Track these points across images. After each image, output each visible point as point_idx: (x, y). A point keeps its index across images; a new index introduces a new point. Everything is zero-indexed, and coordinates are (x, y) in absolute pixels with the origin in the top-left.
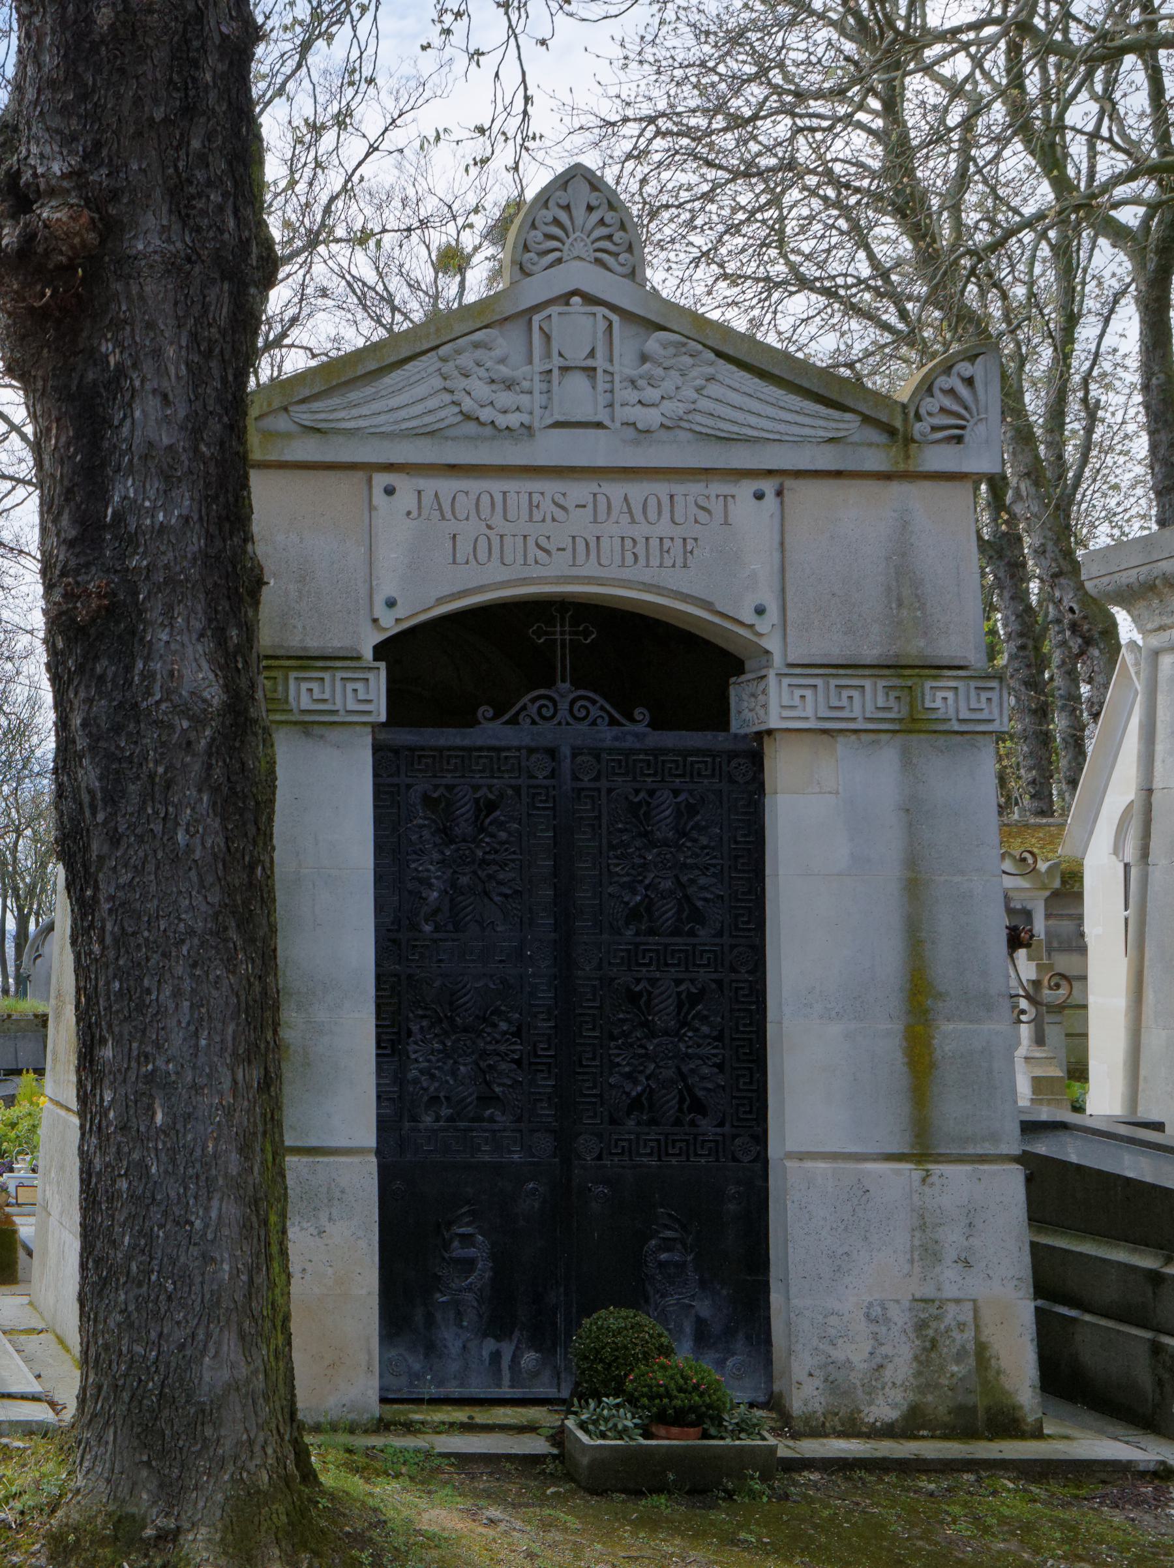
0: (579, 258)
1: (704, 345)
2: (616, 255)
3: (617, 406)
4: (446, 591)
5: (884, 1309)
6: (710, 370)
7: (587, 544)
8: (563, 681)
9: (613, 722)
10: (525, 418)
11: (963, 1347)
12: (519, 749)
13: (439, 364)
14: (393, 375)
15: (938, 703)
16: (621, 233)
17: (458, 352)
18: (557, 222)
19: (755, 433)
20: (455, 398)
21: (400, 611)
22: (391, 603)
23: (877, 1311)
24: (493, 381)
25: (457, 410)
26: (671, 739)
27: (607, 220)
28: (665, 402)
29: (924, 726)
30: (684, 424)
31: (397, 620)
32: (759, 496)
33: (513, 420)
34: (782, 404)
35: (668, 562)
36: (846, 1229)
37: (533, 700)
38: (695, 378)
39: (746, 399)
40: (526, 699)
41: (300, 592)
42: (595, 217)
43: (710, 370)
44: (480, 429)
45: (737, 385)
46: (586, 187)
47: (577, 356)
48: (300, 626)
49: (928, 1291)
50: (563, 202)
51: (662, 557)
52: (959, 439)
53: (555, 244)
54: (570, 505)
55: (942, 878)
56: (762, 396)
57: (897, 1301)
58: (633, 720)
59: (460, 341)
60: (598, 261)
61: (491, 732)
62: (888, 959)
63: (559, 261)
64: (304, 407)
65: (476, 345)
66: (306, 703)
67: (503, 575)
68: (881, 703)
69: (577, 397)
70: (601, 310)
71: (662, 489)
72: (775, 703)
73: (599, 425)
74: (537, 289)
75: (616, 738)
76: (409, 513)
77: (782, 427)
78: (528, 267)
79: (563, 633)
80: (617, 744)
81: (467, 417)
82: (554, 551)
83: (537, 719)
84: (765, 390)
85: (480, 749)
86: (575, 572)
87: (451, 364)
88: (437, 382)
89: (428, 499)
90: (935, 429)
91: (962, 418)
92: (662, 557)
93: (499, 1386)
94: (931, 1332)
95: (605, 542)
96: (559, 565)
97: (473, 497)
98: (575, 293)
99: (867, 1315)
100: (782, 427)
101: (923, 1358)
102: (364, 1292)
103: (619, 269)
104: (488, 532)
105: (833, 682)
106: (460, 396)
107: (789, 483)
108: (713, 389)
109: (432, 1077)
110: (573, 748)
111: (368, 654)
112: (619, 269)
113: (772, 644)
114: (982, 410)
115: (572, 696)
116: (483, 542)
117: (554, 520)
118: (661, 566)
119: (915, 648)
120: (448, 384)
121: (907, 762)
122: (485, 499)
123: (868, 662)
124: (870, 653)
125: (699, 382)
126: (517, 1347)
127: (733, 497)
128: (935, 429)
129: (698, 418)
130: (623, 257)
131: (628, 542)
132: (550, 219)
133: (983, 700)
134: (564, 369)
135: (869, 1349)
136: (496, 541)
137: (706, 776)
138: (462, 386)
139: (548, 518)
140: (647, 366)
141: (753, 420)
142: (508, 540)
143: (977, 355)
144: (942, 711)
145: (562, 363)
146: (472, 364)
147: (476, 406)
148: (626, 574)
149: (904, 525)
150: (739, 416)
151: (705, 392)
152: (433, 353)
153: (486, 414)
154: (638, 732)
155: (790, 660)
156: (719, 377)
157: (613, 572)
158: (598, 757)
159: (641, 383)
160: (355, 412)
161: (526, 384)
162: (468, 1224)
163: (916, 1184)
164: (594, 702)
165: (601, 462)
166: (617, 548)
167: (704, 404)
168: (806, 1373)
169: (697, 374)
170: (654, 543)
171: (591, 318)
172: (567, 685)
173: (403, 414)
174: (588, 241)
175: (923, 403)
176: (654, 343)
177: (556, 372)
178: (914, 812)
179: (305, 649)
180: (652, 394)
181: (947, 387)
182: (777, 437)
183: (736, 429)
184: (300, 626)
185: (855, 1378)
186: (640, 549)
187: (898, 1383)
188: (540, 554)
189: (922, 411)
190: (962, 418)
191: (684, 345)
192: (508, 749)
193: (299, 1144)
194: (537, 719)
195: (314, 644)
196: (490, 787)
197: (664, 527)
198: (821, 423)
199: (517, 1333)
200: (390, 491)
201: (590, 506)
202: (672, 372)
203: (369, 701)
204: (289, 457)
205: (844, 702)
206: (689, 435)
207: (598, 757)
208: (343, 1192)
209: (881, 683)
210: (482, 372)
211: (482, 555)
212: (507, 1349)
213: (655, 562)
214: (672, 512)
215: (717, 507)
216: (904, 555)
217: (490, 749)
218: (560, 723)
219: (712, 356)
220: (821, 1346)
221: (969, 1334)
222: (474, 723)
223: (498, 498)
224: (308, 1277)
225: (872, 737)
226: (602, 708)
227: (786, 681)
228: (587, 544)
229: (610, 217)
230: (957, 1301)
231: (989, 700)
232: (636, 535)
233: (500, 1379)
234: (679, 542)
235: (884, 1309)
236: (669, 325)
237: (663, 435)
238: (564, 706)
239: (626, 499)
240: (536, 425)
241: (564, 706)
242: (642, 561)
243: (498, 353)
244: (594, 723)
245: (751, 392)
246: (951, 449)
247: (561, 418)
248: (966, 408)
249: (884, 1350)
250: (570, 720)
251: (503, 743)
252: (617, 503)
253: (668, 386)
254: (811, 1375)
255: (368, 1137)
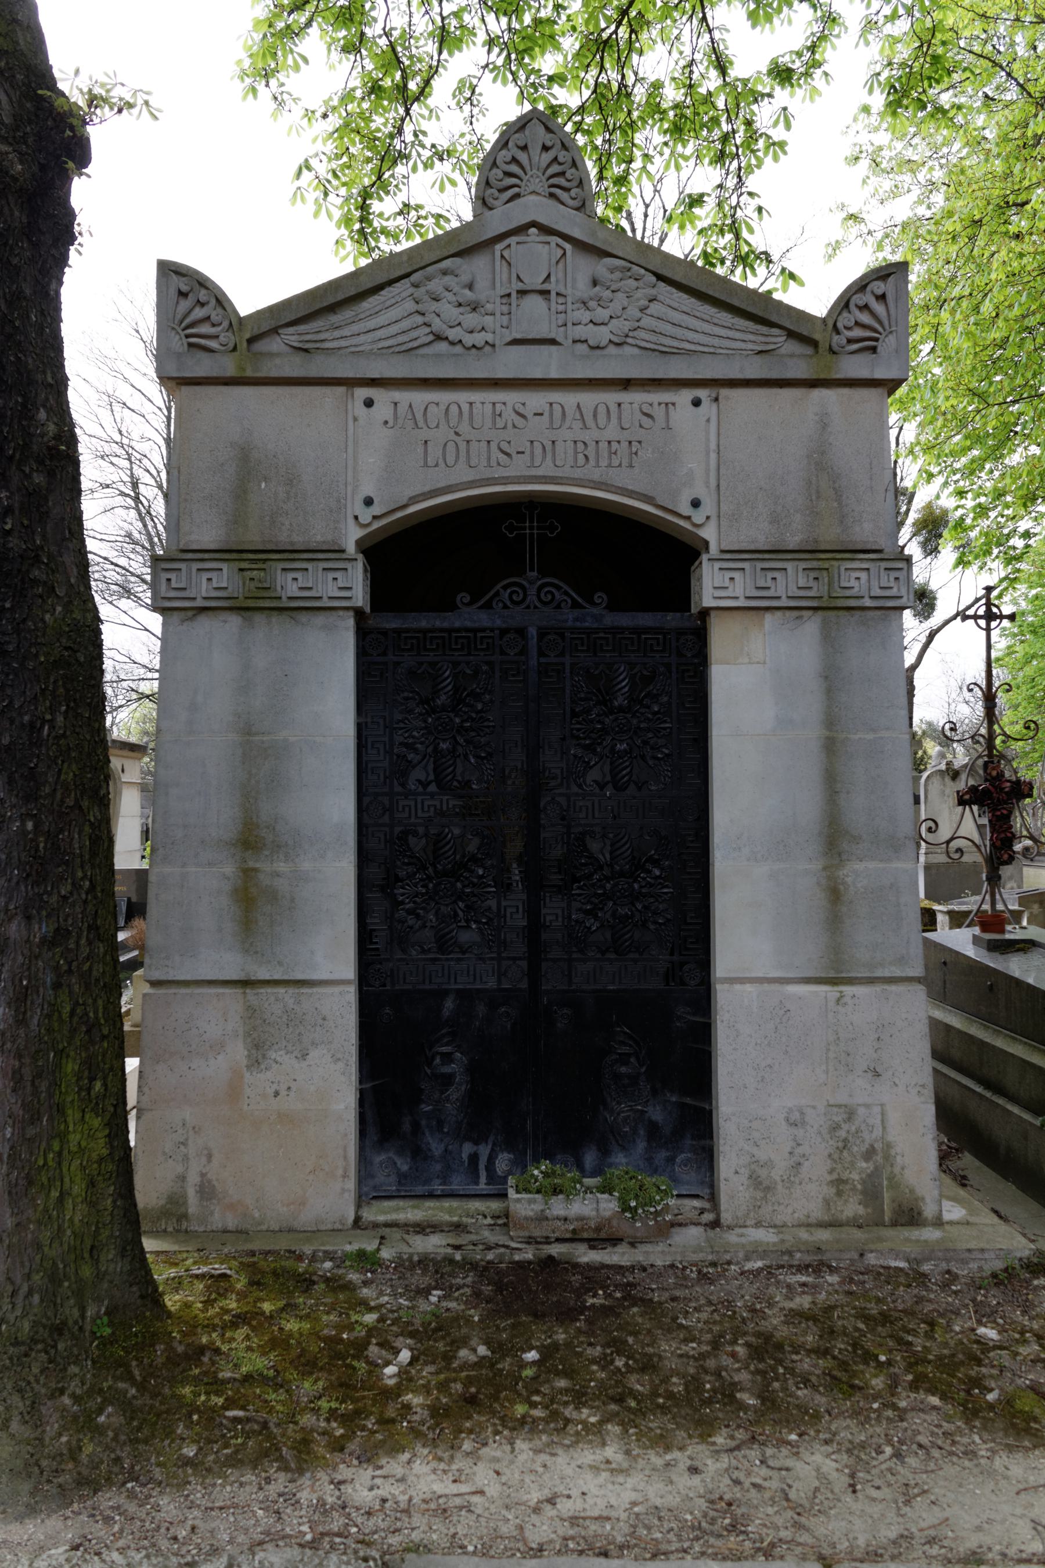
0: (533, 192)
1: (647, 270)
2: (567, 190)
3: (569, 325)
4: (418, 489)
5: (802, 1113)
6: (653, 292)
7: (544, 447)
8: (532, 570)
9: (575, 605)
10: (489, 337)
11: (872, 1146)
12: (492, 630)
13: (412, 290)
14: (371, 300)
15: (853, 583)
16: (573, 170)
17: (429, 279)
18: (514, 160)
19: (692, 347)
20: (426, 319)
21: (376, 509)
22: (369, 502)
23: (796, 1116)
24: (460, 305)
25: (428, 330)
26: (625, 620)
27: (561, 159)
28: (613, 321)
29: (840, 603)
30: (629, 340)
31: (375, 517)
32: (697, 403)
33: (479, 339)
34: (716, 321)
35: (616, 463)
36: (769, 1044)
37: (505, 588)
38: (638, 300)
39: (685, 317)
40: (498, 587)
41: (288, 493)
42: (547, 157)
43: (653, 292)
44: (451, 348)
45: (675, 305)
46: (541, 130)
47: (534, 281)
48: (287, 523)
49: (842, 1098)
50: (521, 143)
51: (610, 458)
52: (874, 350)
53: (514, 181)
54: (528, 412)
55: (857, 737)
56: (698, 314)
57: (814, 1107)
58: (593, 604)
59: (429, 269)
60: (552, 195)
61: (469, 617)
62: (808, 806)
63: (517, 196)
64: (291, 330)
65: (445, 273)
66: (293, 590)
67: (469, 476)
68: (802, 583)
69: (535, 316)
70: (554, 240)
71: (611, 397)
72: (712, 585)
73: (553, 342)
74: (500, 220)
75: (576, 619)
76: (386, 422)
77: (716, 342)
78: (490, 201)
79: (531, 528)
80: (578, 624)
81: (439, 337)
82: (514, 455)
83: (508, 603)
84: (701, 308)
85: (458, 630)
86: (533, 472)
87: (422, 290)
88: (410, 306)
89: (403, 409)
90: (850, 341)
91: (876, 331)
92: (610, 458)
93: (477, 1183)
94: (843, 1134)
95: (559, 445)
96: (518, 467)
97: (443, 407)
98: (534, 224)
99: (787, 1120)
100: (716, 342)
101: (836, 1156)
102: (342, 1106)
103: (571, 202)
104: (456, 438)
105: (760, 565)
106: (430, 318)
107: (724, 392)
108: (655, 308)
109: (418, 916)
110: (539, 628)
111: (351, 548)
112: (571, 202)
113: (708, 533)
114: (893, 323)
115: (539, 583)
116: (451, 447)
117: (514, 426)
118: (609, 466)
119: (829, 535)
120: (420, 307)
121: (828, 639)
122: (454, 409)
123: (791, 548)
124: (793, 541)
125: (644, 302)
126: (492, 1150)
127: (673, 404)
128: (850, 341)
129: (642, 334)
130: (573, 193)
131: (580, 446)
132: (509, 159)
133: (892, 579)
134: (522, 293)
135: (789, 1149)
136: (463, 446)
137: (582, 651)
138: (433, 308)
139: (510, 425)
140: (597, 288)
141: (691, 336)
142: (474, 445)
143: (889, 275)
144: (856, 589)
145: (520, 286)
146: (441, 289)
147: (445, 327)
148: (577, 473)
149: (824, 424)
150: (679, 332)
151: (648, 311)
152: (406, 280)
153: (453, 334)
154: (600, 616)
155: (723, 547)
156: (660, 297)
157: (566, 472)
158: (562, 636)
159: (592, 304)
160: (337, 334)
161: (489, 307)
162: (447, 1044)
163: (832, 1004)
164: (558, 588)
165: (554, 374)
166: (570, 452)
167: (646, 322)
168: (733, 1170)
169: (641, 296)
170: (603, 445)
171: (547, 247)
172: (535, 573)
173: (379, 334)
174: (544, 179)
175: (840, 318)
176: (602, 267)
177: (514, 295)
178: (832, 680)
179: (292, 543)
180: (602, 314)
181: (861, 303)
182: (712, 350)
183: (675, 344)
184: (287, 523)
185: (776, 1175)
186: (591, 451)
187: (814, 1178)
188: (501, 456)
189: (840, 325)
190: (876, 331)
191: (629, 270)
192: (483, 630)
193: (286, 977)
194: (508, 603)
195: (299, 540)
196: (468, 663)
197: (612, 432)
198: (752, 337)
199: (491, 1138)
200: (369, 403)
201: (546, 414)
202: (619, 295)
203: (350, 588)
204: (274, 373)
205: (769, 583)
206: (636, 351)
207: (562, 636)
208: (324, 1019)
209: (803, 565)
210: (450, 296)
211: (450, 460)
212: (484, 1151)
213: (604, 463)
214: (620, 418)
215: (659, 412)
216: (823, 453)
217: (467, 630)
218: (528, 607)
219: (654, 279)
220: (746, 1147)
221: (878, 1132)
222: (453, 607)
223: (465, 408)
224: (292, 1094)
225: (796, 613)
226: (566, 593)
227: (717, 565)
228: (544, 447)
229: (563, 156)
230: (867, 1106)
231: (897, 579)
232: (587, 439)
233: (478, 1177)
234: (625, 445)
235: (802, 1113)
236: (615, 252)
237: (612, 350)
238: (532, 591)
239: (578, 406)
240: (497, 343)
241: (532, 591)
242: (592, 462)
243: (465, 278)
244: (558, 607)
245: (688, 310)
246: (866, 358)
247: (519, 336)
248: (880, 323)
249: (799, 1150)
250: (538, 604)
251: (477, 625)
252: (571, 411)
253: (616, 307)
254: (737, 1172)
255: (348, 970)
